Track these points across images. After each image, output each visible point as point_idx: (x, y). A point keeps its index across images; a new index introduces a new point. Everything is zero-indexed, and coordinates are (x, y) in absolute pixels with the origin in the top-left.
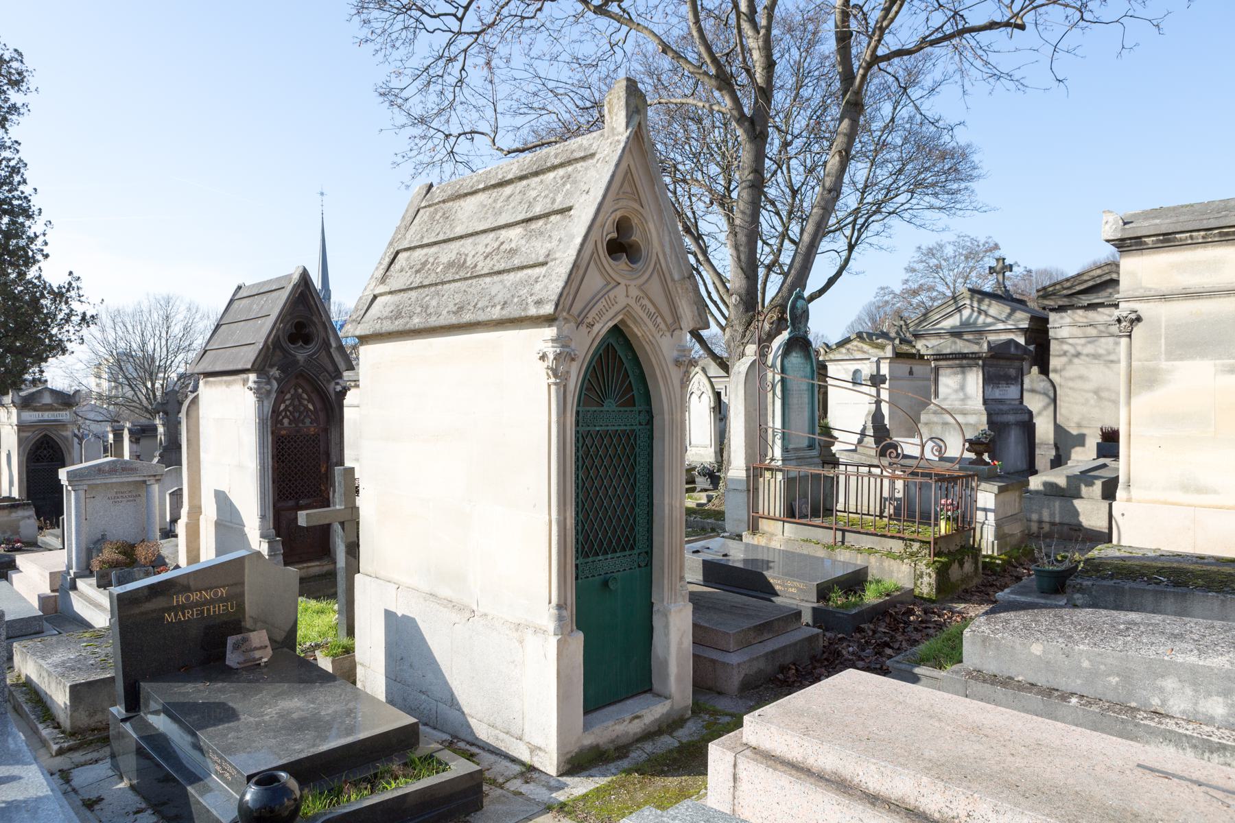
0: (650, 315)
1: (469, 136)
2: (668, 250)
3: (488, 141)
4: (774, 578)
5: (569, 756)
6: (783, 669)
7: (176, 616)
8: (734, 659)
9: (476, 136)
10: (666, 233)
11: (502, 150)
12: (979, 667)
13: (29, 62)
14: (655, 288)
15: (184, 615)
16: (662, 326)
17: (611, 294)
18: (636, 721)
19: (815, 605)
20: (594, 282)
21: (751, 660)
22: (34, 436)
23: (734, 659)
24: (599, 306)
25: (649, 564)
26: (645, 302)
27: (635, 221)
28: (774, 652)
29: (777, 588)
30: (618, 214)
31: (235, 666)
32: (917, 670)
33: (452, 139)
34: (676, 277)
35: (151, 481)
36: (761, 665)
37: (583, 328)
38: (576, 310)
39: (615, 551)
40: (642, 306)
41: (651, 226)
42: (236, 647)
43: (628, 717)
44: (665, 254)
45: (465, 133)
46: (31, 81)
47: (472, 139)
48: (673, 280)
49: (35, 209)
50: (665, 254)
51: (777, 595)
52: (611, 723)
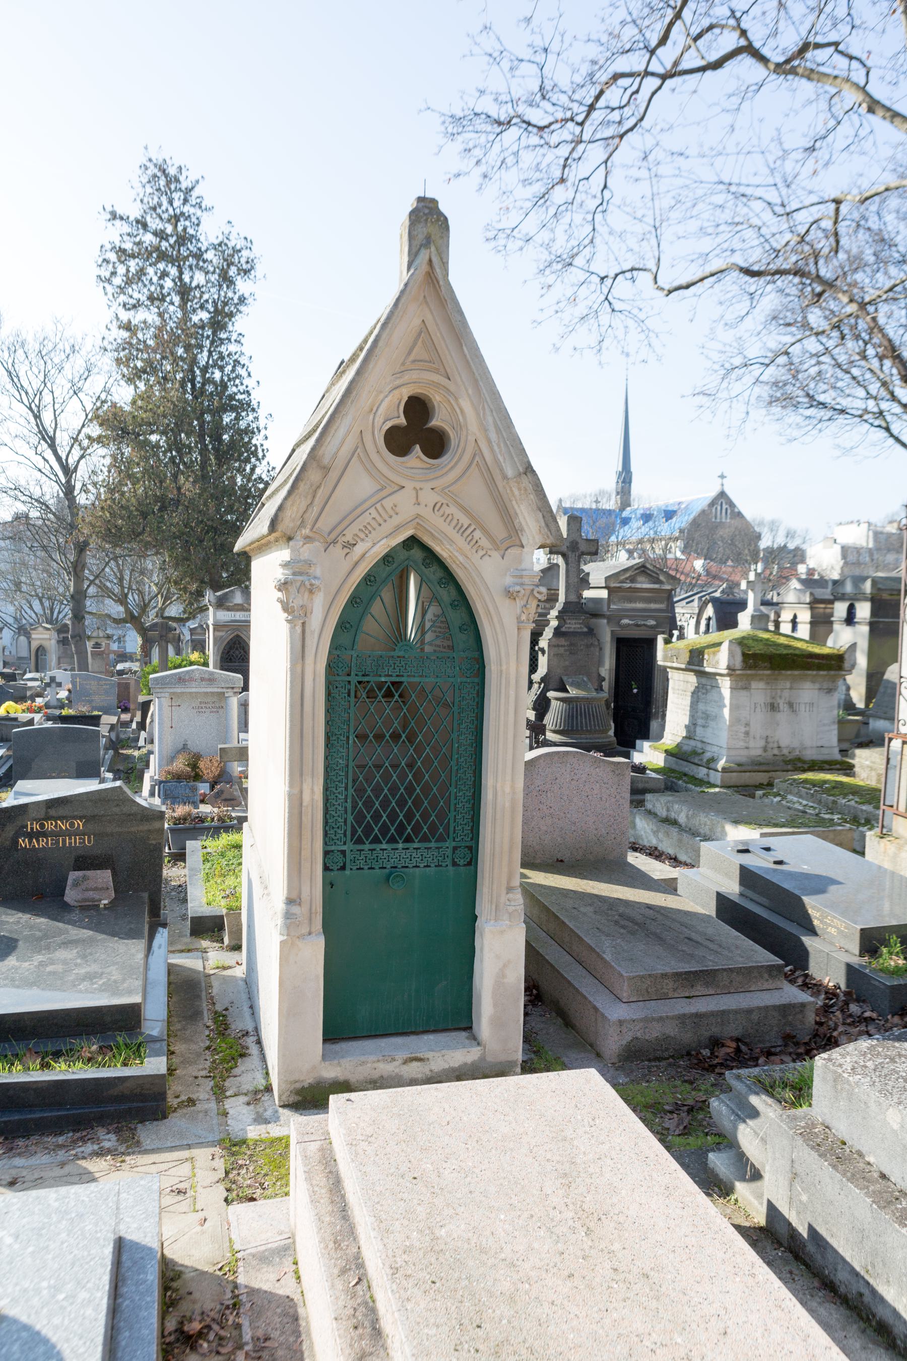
0: (461, 530)
1: (628, 275)
2: (493, 436)
3: (649, 277)
4: (813, 908)
5: (298, 1086)
6: (715, 1043)
7: (30, 843)
8: (616, 1012)
9: (635, 273)
10: (488, 412)
11: (662, 289)
12: (828, 1122)
13: (256, 251)
14: (474, 491)
15: (38, 842)
16: (484, 542)
17: (388, 503)
18: (415, 1064)
19: (855, 960)
20: (358, 486)
21: (646, 1020)
22: (227, 636)
23: (616, 1012)
24: (366, 518)
25: (472, 861)
26: (453, 510)
27: (436, 398)
28: (698, 1015)
29: (816, 922)
30: (405, 393)
31: (72, 903)
32: (754, 1100)
33: (608, 282)
34: (510, 473)
35: (229, 693)
36: (671, 1030)
37: (337, 551)
38: (325, 523)
39: (408, 840)
40: (447, 518)
41: (466, 404)
42: (76, 884)
43: (402, 1055)
44: (489, 441)
45: (623, 272)
46: (259, 271)
47: (633, 280)
48: (505, 477)
49: (254, 403)
50: (489, 441)
51: (813, 932)
52: (372, 1058)
